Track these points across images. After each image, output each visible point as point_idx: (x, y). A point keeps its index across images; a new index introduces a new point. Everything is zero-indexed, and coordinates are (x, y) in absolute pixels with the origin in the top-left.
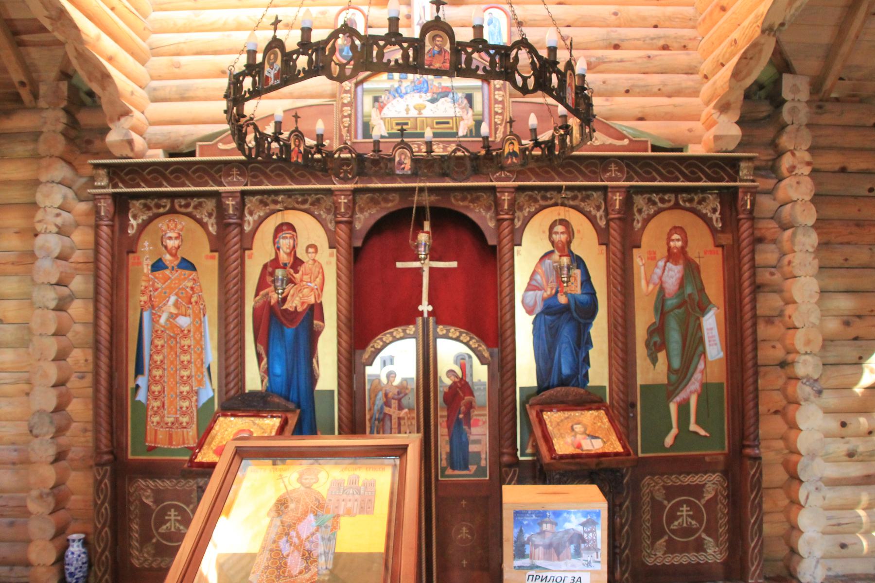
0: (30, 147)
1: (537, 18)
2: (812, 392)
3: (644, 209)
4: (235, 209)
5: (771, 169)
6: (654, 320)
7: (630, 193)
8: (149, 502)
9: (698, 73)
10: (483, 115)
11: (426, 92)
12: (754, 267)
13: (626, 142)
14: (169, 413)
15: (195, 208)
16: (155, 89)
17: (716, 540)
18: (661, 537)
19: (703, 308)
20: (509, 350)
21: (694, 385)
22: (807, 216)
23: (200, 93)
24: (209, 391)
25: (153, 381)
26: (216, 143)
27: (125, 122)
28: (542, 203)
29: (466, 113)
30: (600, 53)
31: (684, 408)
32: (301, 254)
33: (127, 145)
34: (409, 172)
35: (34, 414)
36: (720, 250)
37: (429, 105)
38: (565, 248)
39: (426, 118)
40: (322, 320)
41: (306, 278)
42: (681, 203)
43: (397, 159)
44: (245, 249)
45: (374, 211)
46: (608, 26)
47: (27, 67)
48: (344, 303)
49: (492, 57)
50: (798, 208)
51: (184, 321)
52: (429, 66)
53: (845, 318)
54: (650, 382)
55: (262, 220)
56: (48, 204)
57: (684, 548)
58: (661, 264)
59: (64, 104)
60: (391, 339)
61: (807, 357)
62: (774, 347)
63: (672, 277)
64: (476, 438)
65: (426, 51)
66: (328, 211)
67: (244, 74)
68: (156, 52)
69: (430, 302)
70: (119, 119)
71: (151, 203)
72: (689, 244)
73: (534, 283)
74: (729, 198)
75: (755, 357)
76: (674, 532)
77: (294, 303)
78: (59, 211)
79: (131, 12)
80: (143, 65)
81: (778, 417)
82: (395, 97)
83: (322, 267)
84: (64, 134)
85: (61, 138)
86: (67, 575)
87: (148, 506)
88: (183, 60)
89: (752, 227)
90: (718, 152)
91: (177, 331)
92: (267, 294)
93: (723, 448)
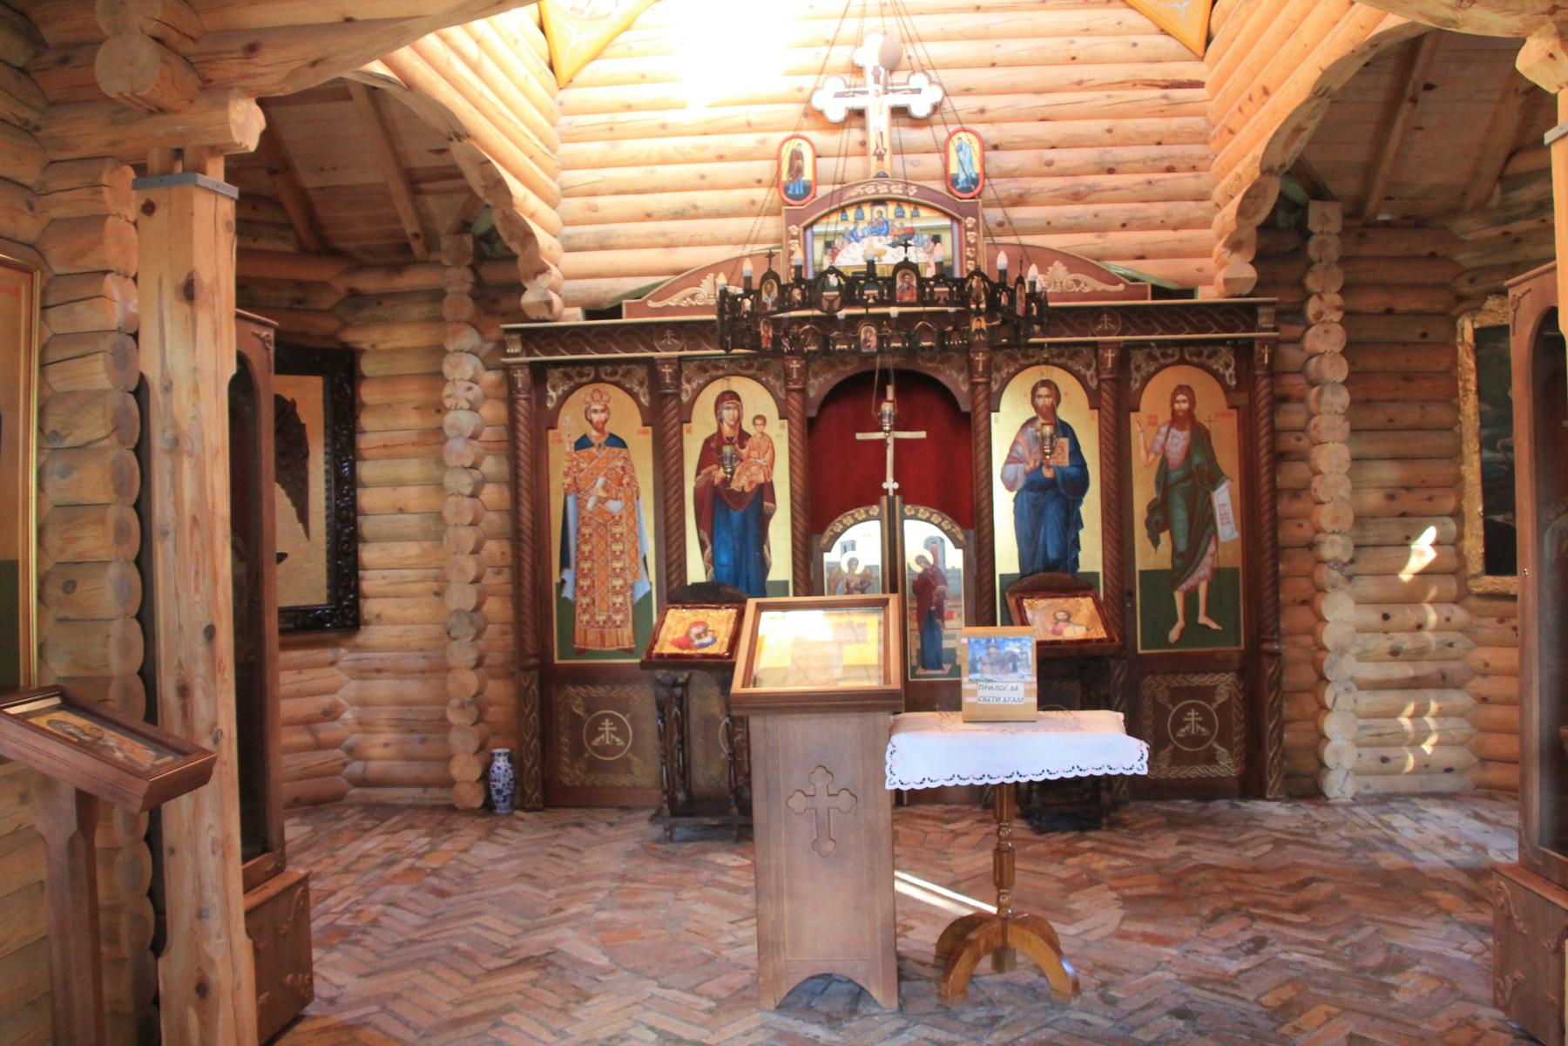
0: (426, 308)
1: (1016, 140)
2: (1342, 578)
3: (1143, 365)
4: (672, 377)
5: (1293, 314)
6: (1155, 495)
7: (1124, 352)
8: (579, 711)
10: (953, 260)
11: (886, 234)
12: (1274, 432)
13: (1121, 287)
14: (600, 610)
15: (624, 376)
16: (569, 237)
17: (1230, 749)
18: (1165, 747)
19: (1215, 479)
20: (986, 531)
21: (1204, 570)
22: (1336, 371)
23: (623, 241)
24: (648, 582)
25: (580, 574)
26: (645, 301)
27: (543, 281)
28: (1022, 361)
31: (1191, 597)
32: (747, 426)
33: (545, 307)
35: (450, 614)
36: (1234, 412)
37: (890, 249)
38: (1049, 413)
40: (773, 500)
41: (754, 454)
42: (1187, 357)
43: (863, 337)
44: (682, 423)
45: (829, 376)
46: (1101, 145)
47: (422, 217)
48: (798, 481)
50: (1326, 362)
51: (614, 506)
53: (1390, 490)
54: (1151, 568)
55: (701, 388)
56: (457, 376)
57: (1193, 760)
58: (1164, 430)
59: (470, 260)
60: (852, 521)
61: (1335, 537)
62: (1300, 526)
63: (1176, 445)
64: (950, 632)
66: (777, 377)
68: (568, 192)
69: (896, 479)
70: (535, 277)
71: (572, 371)
72: (1197, 406)
73: (1014, 454)
74: (1244, 351)
75: (1275, 536)
76: (1180, 740)
77: (741, 483)
78: (470, 384)
81: (1306, 608)
82: (850, 242)
83: (771, 442)
84: (471, 294)
85: (469, 301)
86: (493, 793)
87: (579, 716)
88: (600, 201)
89: (1271, 384)
91: (607, 517)
92: (710, 473)
93: (1238, 644)
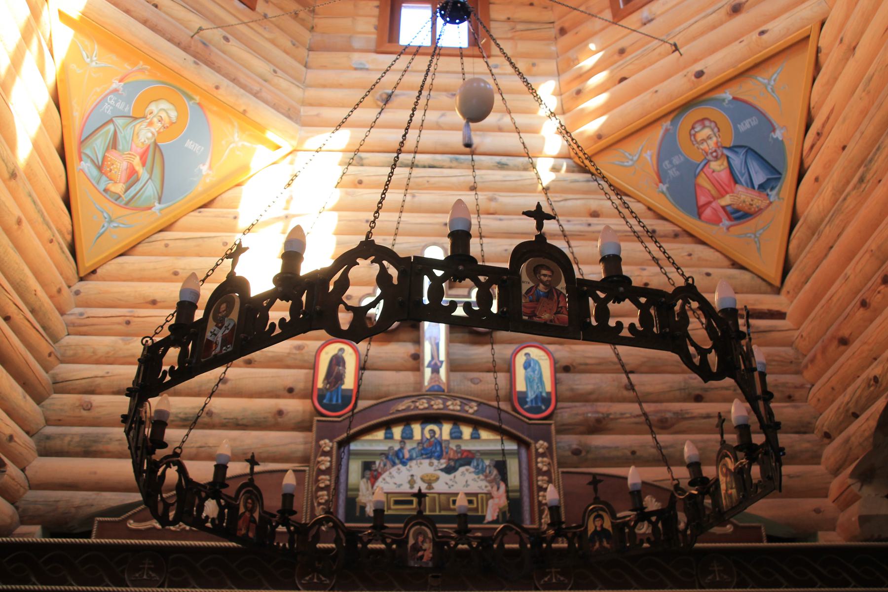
1: (589, 361)
9: (813, 432)
10: (520, 490)
11: (439, 458)
16: (48, 438)
29: (495, 488)
30: (677, 406)
34: (430, 564)
39: (439, 494)
43: (411, 541)
49: (644, 308)
52: (530, 317)
65: (524, 290)
67: (166, 344)
68: (61, 386)
79: (35, 328)
80: (38, 404)
82: (394, 464)
88: (96, 399)
90: (866, 540)
